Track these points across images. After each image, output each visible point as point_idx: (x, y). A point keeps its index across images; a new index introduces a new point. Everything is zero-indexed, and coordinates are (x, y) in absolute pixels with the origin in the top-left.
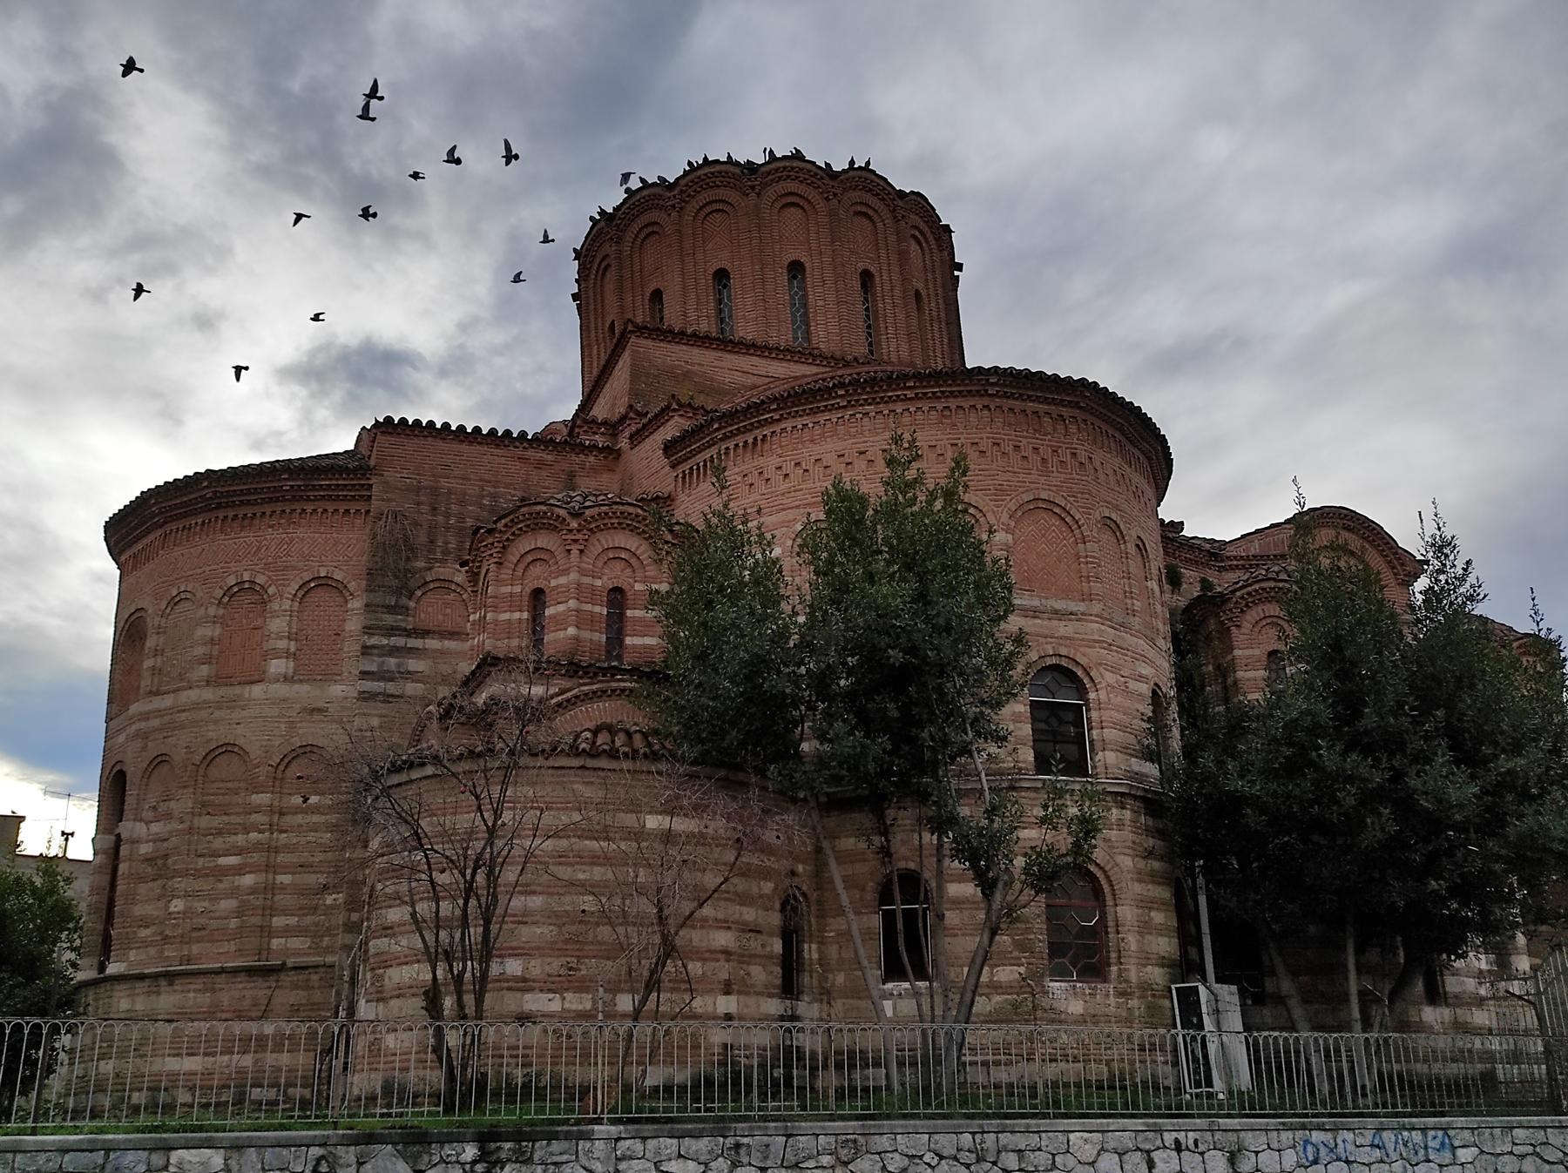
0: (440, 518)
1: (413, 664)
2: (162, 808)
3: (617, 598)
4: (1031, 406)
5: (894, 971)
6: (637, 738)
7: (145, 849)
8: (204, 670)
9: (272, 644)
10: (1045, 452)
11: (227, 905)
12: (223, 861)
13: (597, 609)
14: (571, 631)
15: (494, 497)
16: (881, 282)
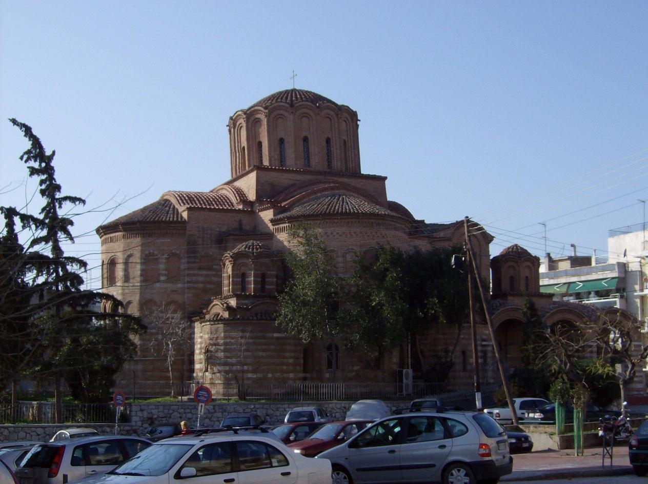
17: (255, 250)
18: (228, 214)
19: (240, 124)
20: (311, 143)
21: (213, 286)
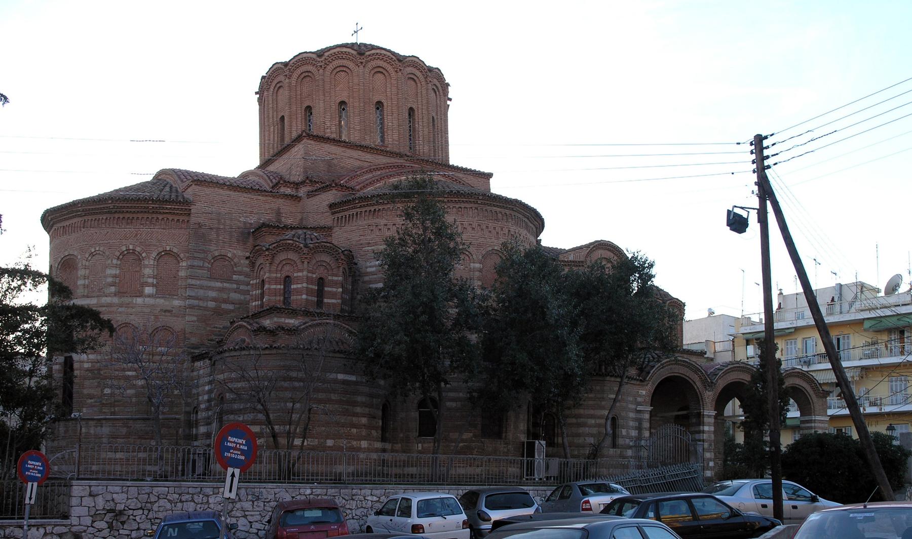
3: (321, 282)
7: (86, 365)
8: (113, 289)
14: (304, 297)
16: (418, 115)
18: (260, 197)
21: (231, 307)
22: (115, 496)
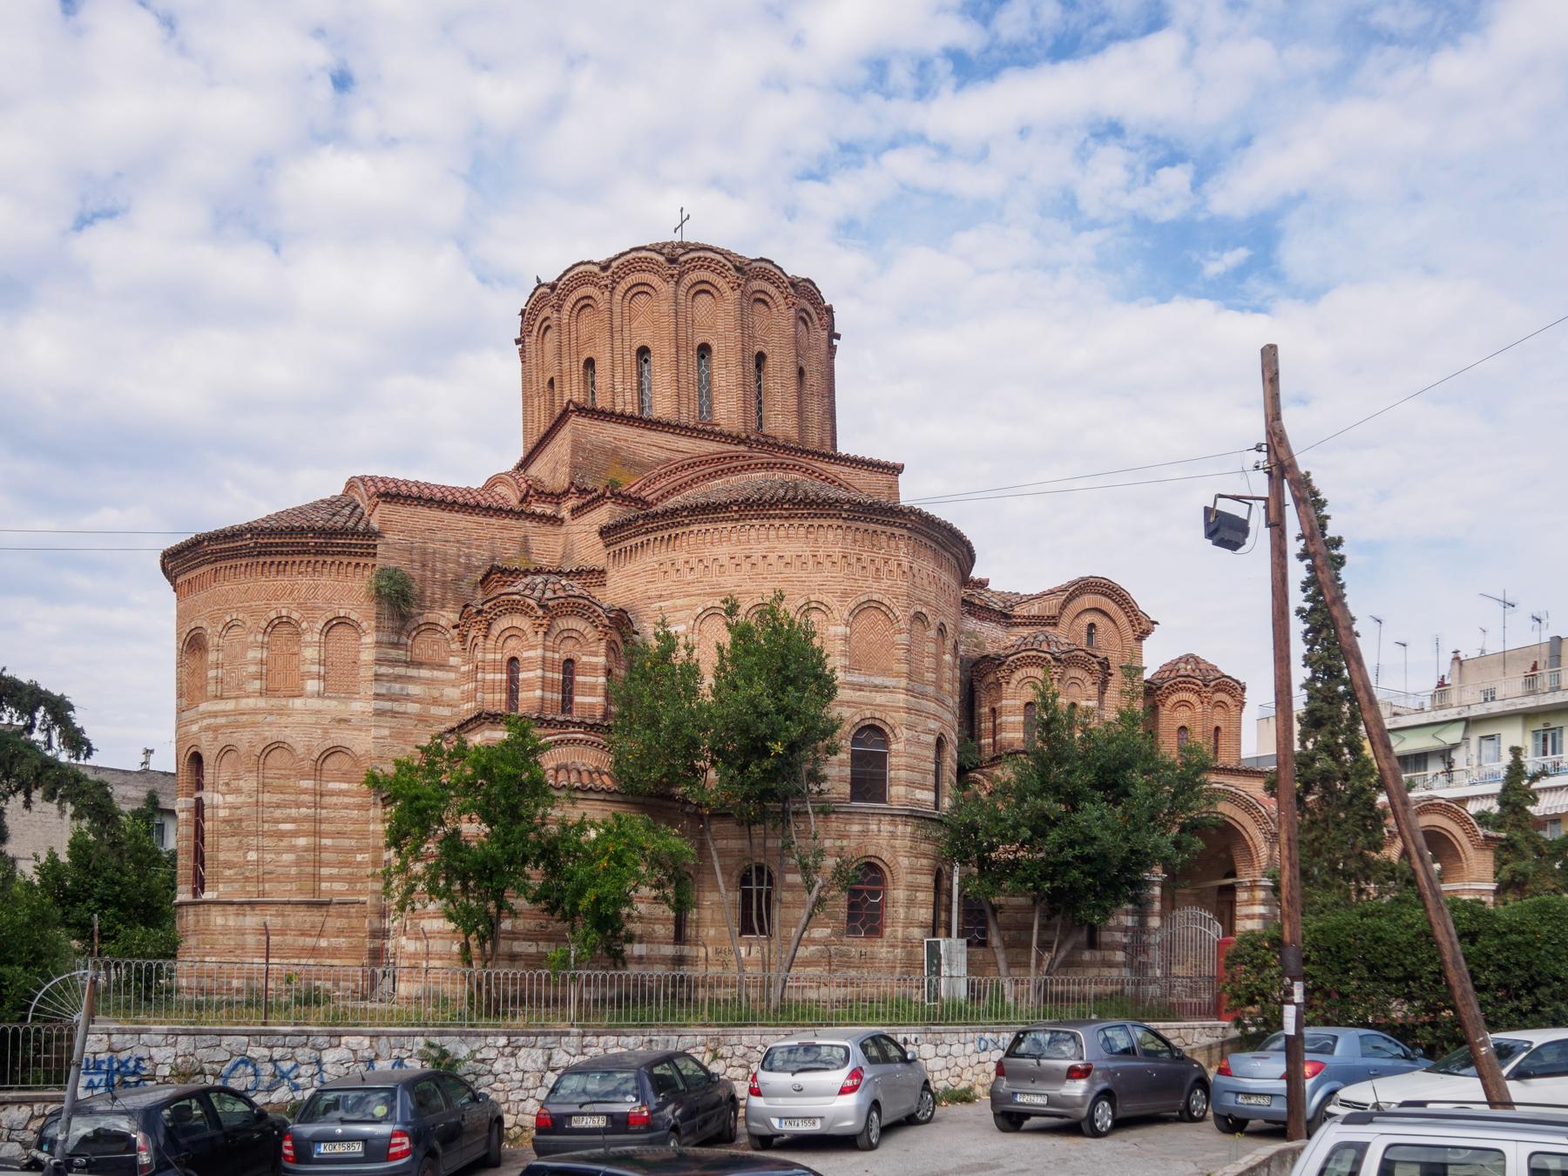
0: (429, 574)
1: (413, 689)
2: (234, 784)
3: (569, 666)
4: (872, 527)
5: (746, 928)
6: (585, 775)
7: (223, 813)
8: (257, 684)
9: (304, 668)
10: (879, 563)
11: (288, 857)
12: (283, 827)
13: (556, 676)
15: (468, 556)
17: (549, 594)
18: (493, 521)
19: (547, 319)
20: (717, 358)
22: (154, 1051)
